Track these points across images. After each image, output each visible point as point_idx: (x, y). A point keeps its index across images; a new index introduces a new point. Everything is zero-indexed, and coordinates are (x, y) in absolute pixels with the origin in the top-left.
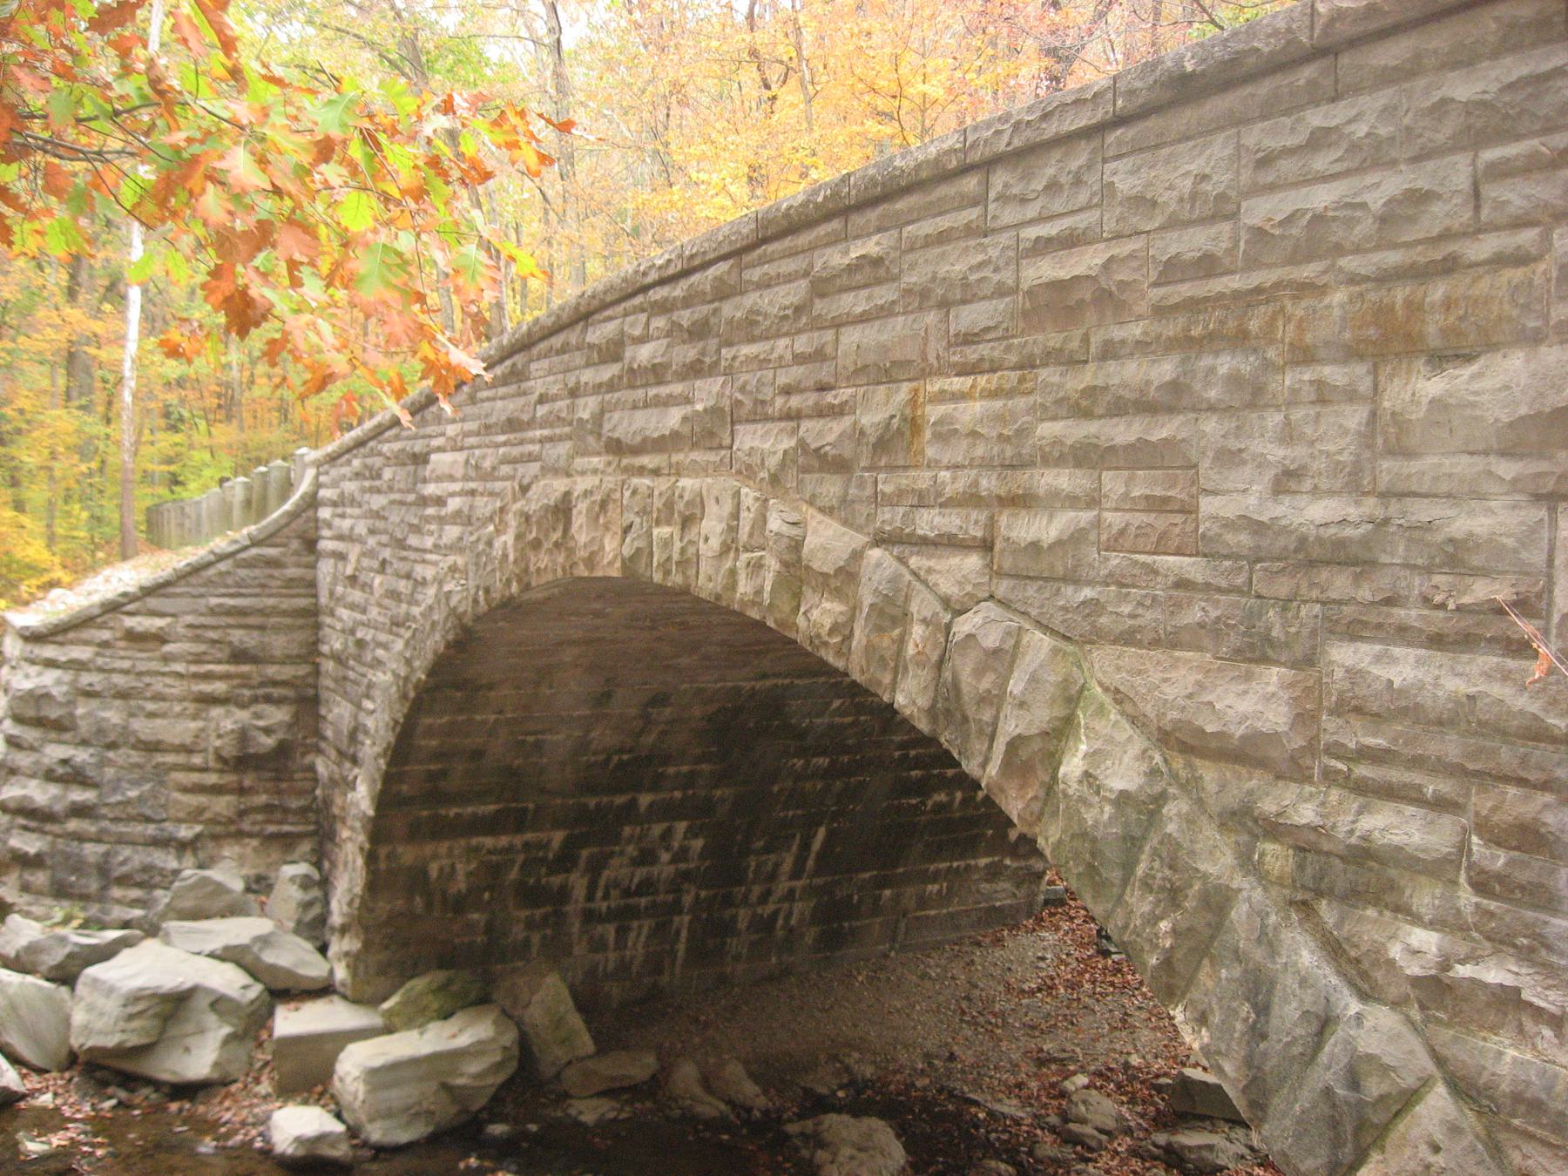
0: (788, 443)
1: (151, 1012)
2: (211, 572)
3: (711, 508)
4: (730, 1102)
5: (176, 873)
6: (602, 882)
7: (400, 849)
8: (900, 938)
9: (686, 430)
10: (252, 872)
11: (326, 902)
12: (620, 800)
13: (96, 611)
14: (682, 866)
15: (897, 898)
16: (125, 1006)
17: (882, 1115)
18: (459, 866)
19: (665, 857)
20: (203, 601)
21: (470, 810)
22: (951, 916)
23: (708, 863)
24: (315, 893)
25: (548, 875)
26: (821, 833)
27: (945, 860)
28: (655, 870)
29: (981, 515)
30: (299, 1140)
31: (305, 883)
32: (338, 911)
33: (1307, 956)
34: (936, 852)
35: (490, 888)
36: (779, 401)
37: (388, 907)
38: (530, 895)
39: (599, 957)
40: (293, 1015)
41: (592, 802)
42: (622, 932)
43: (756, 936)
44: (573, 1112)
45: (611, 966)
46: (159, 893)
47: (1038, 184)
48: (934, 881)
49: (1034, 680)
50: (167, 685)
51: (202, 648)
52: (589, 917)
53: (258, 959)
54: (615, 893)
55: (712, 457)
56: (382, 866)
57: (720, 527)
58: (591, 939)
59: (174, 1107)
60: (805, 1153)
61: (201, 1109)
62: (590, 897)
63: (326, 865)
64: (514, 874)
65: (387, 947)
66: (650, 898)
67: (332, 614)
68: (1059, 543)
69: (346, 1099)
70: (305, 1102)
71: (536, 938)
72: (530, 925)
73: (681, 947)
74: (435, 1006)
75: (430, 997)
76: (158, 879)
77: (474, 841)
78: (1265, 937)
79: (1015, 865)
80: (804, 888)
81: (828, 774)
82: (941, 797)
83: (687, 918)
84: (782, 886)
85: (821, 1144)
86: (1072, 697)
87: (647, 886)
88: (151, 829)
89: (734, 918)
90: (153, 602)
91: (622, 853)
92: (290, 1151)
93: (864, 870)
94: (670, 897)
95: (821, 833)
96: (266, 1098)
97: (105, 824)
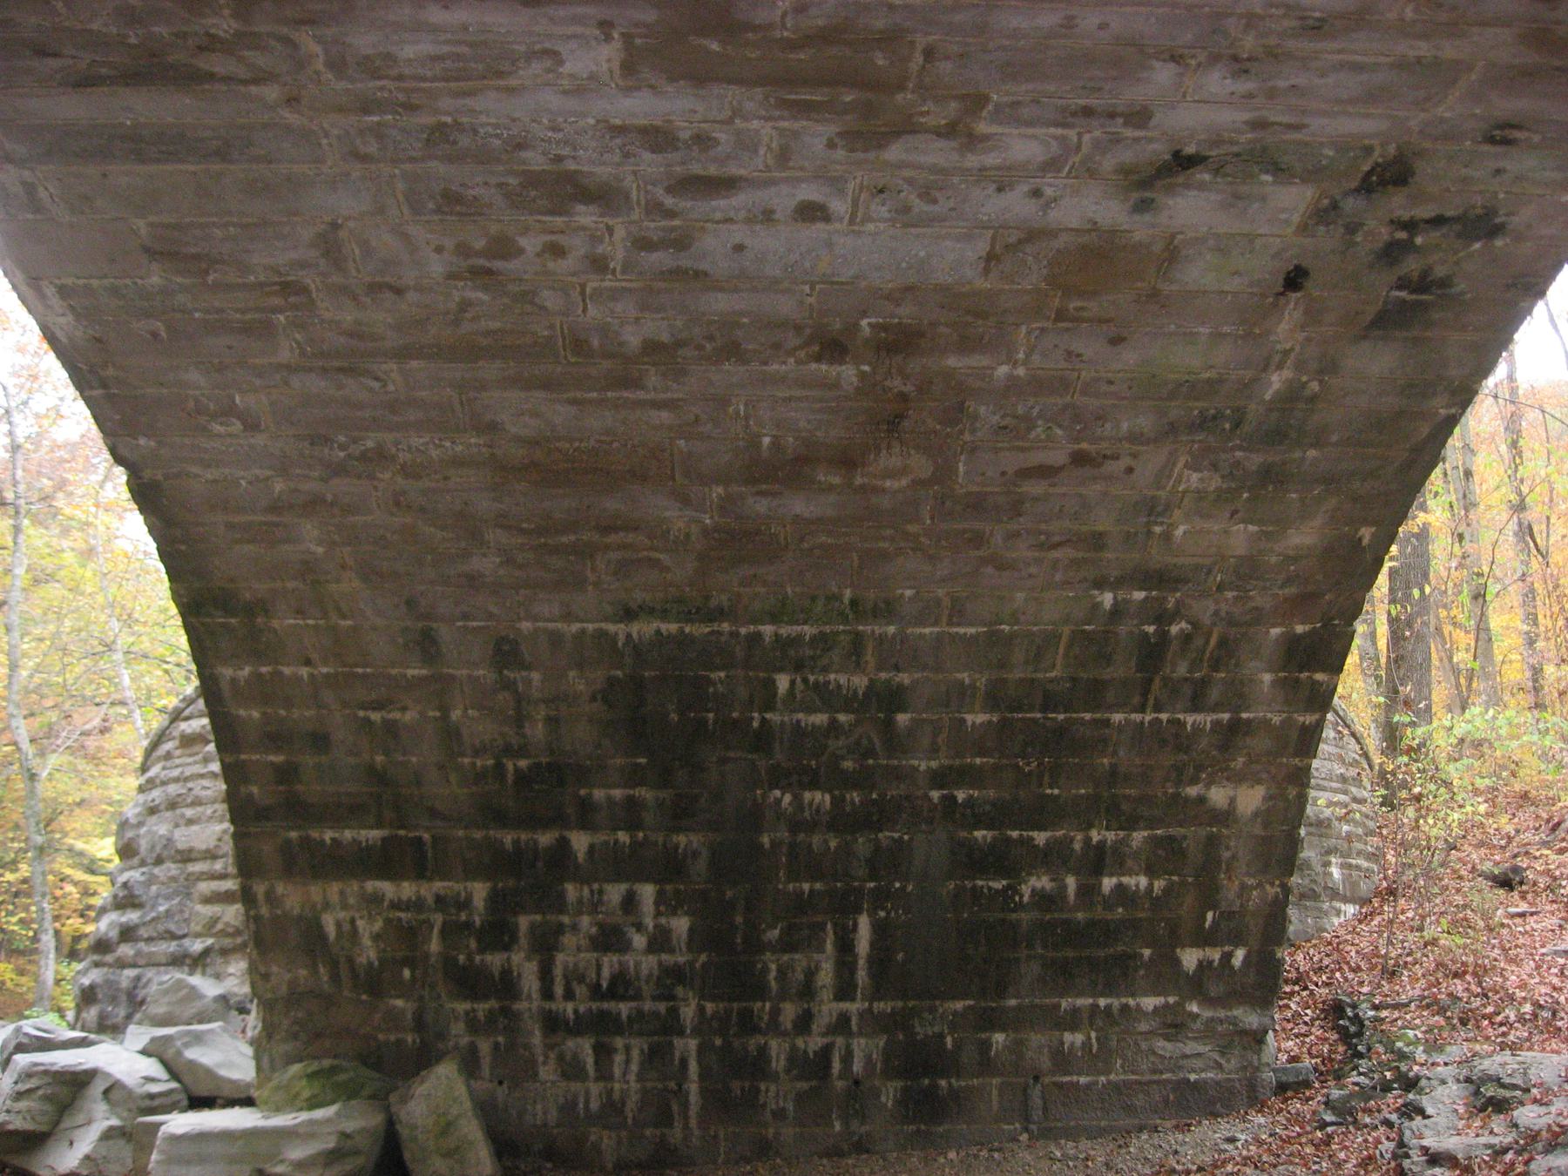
1: (40, 1092)
6: (558, 971)
8: (1037, 1115)
12: (545, 839)
15: (1017, 1047)
16: (16, 1083)
18: (360, 923)
21: (348, 834)
22: (1117, 1088)
23: (703, 958)
25: (482, 951)
26: (864, 924)
27: (1080, 994)
28: (630, 959)
34: (1063, 975)
35: (409, 962)
37: (288, 976)
38: (469, 982)
39: (576, 1086)
41: (508, 838)
42: (603, 1052)
43: (803, 1085)
45: (594, 1105)
48: (1074, 1028)
50: (205, 788)
52: (552, 1023)
53: (179, 1053)
54: (580, 990)
58: (561, 1058)
62: (547, 994)
65: (295, 1036)
66: (633, 1004)
72: (473, 1025)
74: (306, 1094)
75: (304, 1082)
77: (371, 885)
79: (1208, 1014)
80: (861, 1015)
81: (840, 821)
82: (1042, 882)
87: (621, 986)
88: (172, 947)
89: (763, 1051)
91: (575, 928)
93: (954, 998)
94: (662, 1007)
95: (864, 924)
97: (142, 945)
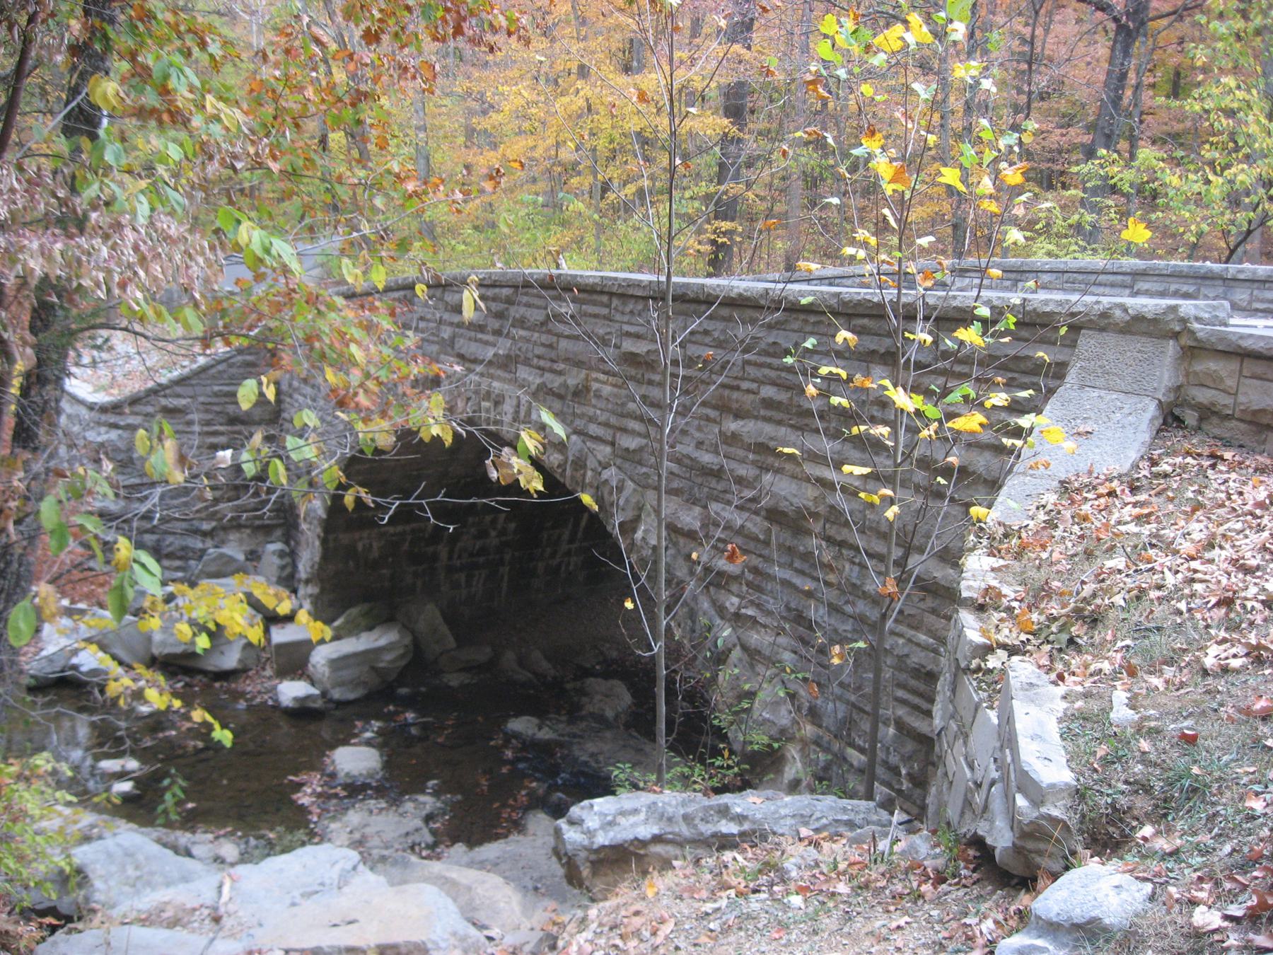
0: (538, 381)
2: (213, 371)
3: (507, 400)
4: (535, 673)
5: (203, 551)
7: (341, 536)
9: (495, 360)
10: (248, 548)
11: (295, 566)
13: (142, 394)
14: (504, 539)
17: (622, 679)
19: (493, 533)
20: (208, 389)
24: (288, 560)
29: (610, 431)
30: (296, 699)
31: (281, 554)
32: (304, 570)
33: (706, 605)
36: (535, 360)
40: (281, 631)
44: (445, 680)
46: (192, 563)
47: (628, 309)
49: (627, 501)
51: (210, 416)
52: (450, 570)
55: (507, 375)
56: (331, 545)
57: (512, 410)
59: (217, 685)
60: (576, 699)
61: (233, 685)
62: (450, 558)
63: (292, 543)
64: (406, 546)
67: (291, 396)
68: (634, 451)
69: (317, 677)
70: (293, 679)
71: (419, 583)
73: (505, 585)
76: (191, 554)
78: (695, 598)
83: (507, 569)
84: (564, 547)
85: (586, 694)
86: (640, 508)
87: (483, 551)
90: (178, 389)
92: (291, 705)
96: (270, 678)
